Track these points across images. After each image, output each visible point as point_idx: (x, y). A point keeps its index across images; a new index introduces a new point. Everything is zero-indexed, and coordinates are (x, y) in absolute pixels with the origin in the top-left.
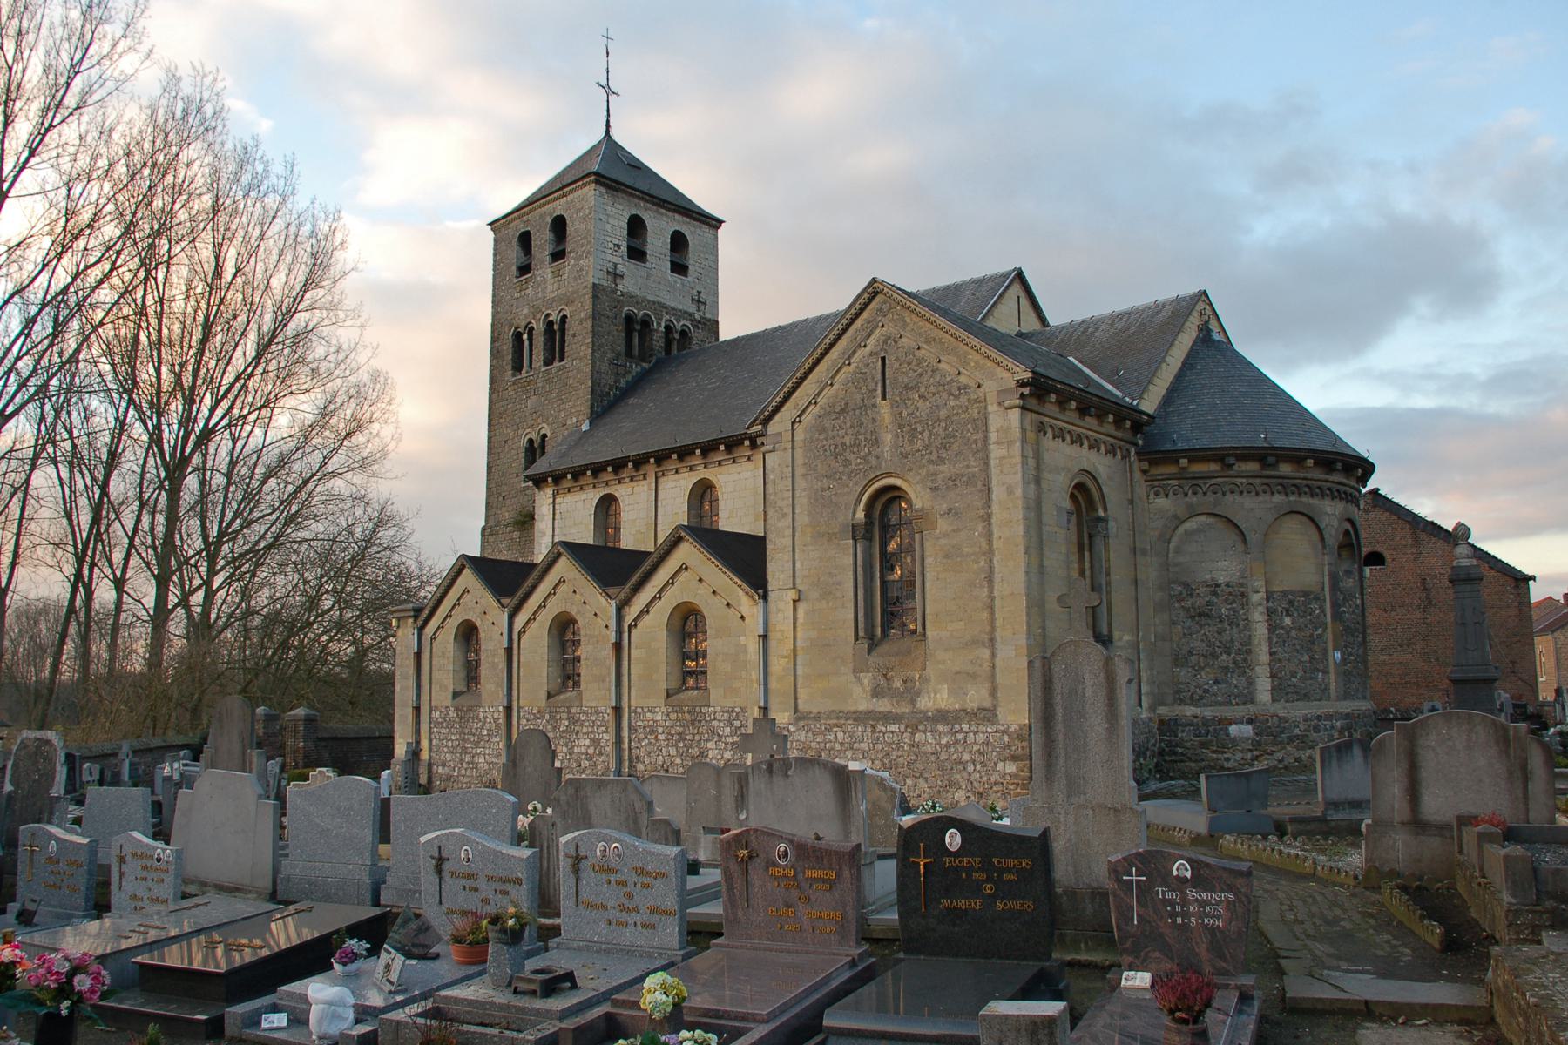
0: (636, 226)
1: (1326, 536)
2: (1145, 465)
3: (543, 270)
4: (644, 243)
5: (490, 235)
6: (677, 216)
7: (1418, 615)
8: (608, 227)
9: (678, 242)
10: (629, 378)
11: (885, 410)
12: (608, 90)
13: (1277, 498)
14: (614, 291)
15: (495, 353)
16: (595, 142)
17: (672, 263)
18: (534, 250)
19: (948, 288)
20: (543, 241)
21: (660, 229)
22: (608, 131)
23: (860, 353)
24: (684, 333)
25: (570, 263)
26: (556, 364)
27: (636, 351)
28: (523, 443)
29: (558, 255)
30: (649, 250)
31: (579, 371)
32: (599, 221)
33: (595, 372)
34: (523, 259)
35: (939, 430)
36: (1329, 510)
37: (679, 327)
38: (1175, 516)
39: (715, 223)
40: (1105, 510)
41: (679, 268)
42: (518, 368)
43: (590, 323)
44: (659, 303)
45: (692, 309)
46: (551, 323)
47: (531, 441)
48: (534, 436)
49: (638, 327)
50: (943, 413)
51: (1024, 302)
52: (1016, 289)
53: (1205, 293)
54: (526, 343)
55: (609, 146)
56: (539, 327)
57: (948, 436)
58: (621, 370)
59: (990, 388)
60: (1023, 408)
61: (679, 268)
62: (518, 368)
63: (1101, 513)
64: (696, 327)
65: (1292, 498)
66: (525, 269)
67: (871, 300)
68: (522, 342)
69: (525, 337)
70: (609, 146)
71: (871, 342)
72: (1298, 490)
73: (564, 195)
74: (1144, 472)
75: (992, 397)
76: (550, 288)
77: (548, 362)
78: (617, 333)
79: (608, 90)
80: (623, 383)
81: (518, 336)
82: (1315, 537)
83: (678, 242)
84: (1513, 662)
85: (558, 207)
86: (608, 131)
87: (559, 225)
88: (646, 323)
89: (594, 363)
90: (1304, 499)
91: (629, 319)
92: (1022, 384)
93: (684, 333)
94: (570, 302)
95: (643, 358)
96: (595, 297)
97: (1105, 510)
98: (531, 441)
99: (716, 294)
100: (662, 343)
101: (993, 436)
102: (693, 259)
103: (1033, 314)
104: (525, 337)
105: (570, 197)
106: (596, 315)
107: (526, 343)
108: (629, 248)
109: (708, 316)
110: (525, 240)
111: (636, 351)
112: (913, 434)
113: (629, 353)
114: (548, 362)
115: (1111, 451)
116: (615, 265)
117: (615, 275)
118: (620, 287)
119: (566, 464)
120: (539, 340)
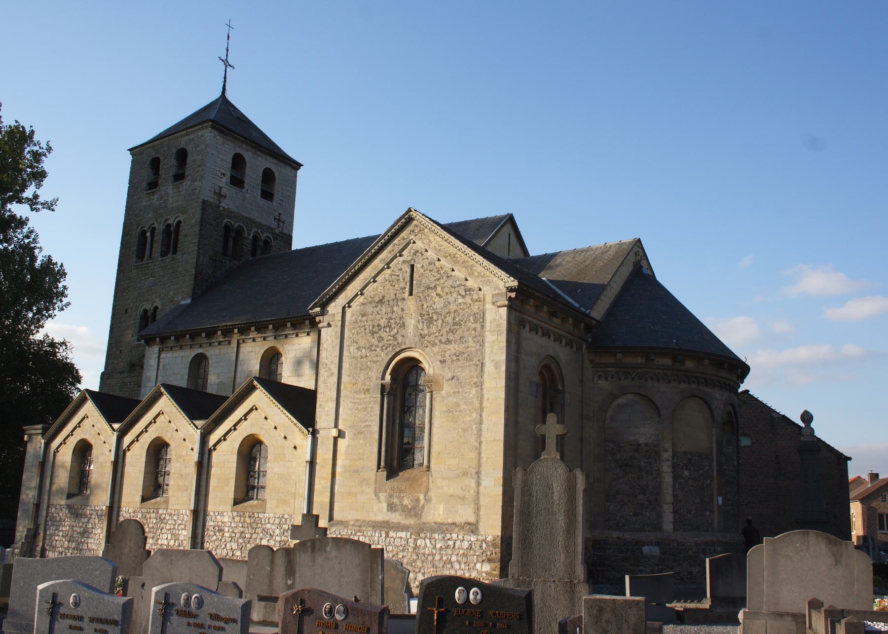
0: (238, 162)
3: (168, 188)
4: (243, 174)
5: (129, 158)
9: (268, 176)
12: (226, 63)
13: (683, 386)
14: (218, 207)
17: (262, 190)
20: (169, 166)
21: (256, 165)
24: (266, 242)
25: (186, 184)
26: (170, 255)
28: (140, 312)
29: (179, 177)
30: (247, 180)
33: (198, 265)
34: (152, 177)
35: (449, 319)
36: (718, 396)
37: (263, 237)
40: (563, 385)
41: (267, 195)
42: (140, 256)
43: (197, 228)
44: (250, 219)
45: (273, 224)
47: (146, 311)
49: (233, 235)
50: (453, 307)
51: (513, 238)
52: (508, 228)
54: (149, 239)
56: (160, 227)
61: (267, 195)
64: (275, 239)
65: (693, 386)
66: (153, 185)
68: (146, 237)
69: (148, 234)
75: (489, 299)
76: (170, 201)
77: (164, 254)
79: (226, 63)
81: (143, 233)
83: (268, 176)
85: (183, 142)
87: (182, 156)
88: (239, 232)
89: (198, 257)
91: (227, 228)
93: (266, 242)
96: (204, 210)
97: (563, 385)
98: (146, 311)
101: (488, 325)
102: (278, 189)
104: (148, 234)
105: (191, 137)
107: (149, 239)
108: (232, 177)
109: (285, 231)
110: (155, 164)
111: (230, 252)
112: (430, 321)
113: (225, 253)
114: (164, 254)
117: (220, 195)
118: (223, 204)
120: (159, 237)
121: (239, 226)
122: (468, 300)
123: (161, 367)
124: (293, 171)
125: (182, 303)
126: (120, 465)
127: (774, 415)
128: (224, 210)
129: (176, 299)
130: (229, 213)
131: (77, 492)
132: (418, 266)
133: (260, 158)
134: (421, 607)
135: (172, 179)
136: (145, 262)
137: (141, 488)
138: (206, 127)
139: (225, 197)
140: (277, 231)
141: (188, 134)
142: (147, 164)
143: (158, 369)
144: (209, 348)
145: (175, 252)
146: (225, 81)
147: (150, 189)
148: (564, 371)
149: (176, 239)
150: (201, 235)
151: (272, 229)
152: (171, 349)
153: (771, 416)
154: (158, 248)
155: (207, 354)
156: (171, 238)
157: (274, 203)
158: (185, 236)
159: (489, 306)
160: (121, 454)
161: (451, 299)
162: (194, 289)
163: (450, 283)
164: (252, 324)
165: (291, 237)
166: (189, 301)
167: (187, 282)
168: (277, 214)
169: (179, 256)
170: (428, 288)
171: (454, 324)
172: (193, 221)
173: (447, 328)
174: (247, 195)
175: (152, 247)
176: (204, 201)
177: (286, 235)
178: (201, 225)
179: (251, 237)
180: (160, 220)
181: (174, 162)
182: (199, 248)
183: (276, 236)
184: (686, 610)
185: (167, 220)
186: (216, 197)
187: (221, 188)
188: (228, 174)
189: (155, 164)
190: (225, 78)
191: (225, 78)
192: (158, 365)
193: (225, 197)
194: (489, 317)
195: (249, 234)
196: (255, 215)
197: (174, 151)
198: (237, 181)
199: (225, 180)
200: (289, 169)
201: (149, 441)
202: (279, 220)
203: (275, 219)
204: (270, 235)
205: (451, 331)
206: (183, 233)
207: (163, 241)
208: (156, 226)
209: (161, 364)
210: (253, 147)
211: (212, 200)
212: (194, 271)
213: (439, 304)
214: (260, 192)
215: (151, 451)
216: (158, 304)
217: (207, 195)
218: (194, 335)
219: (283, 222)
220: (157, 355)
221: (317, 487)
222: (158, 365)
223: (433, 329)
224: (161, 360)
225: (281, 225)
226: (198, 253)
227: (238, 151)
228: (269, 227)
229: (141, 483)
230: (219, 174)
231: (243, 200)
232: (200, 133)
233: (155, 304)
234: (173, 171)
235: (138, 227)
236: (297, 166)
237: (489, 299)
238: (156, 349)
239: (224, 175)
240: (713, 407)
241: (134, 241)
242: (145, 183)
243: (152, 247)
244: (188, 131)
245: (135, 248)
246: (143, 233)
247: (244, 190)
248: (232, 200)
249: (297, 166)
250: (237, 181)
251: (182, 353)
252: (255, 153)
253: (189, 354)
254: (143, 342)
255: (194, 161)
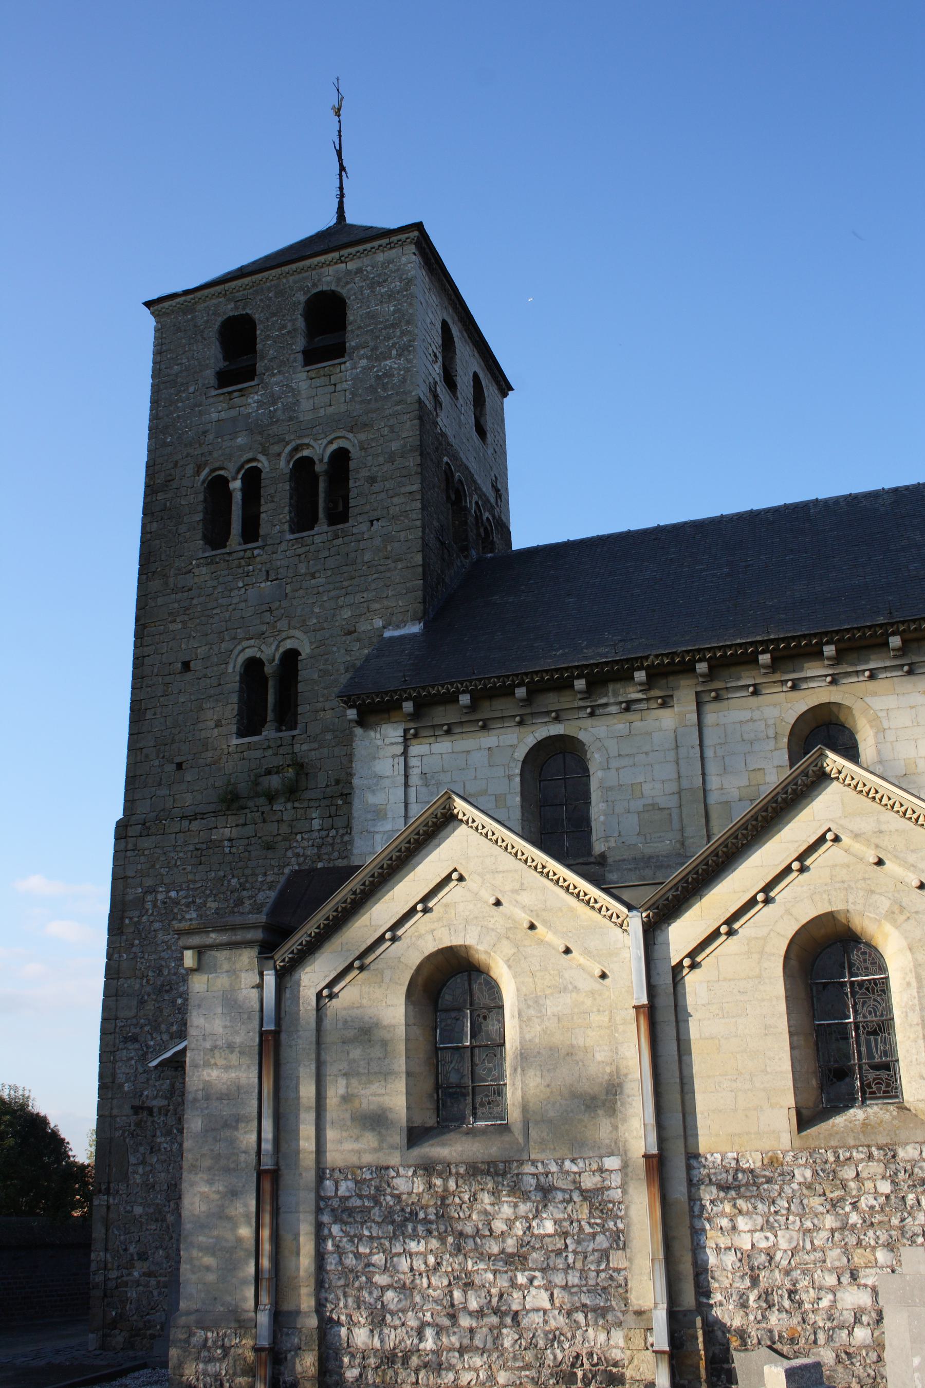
5: (148, 322)
26: (322, 526)
28: (235, 666)
47: (253, 666)
56: (276, 467)
68: (229, 494)
76: (306, 405)
81: (217, 487)
123: (414, 780)
125: (387, 634)
126: (666, 1015)
129: (363, 627)
131: (431, 1121)
134: (342, 1361)
137: (787, 1082)
138: (402, 243)
141: (340, 260)
142: (212, 333)
143: (406, 785)
144: (589, 722)
146: (342, 195)
147: (220, 386)
152: (448, 732)
155: (582, 736)
158: (372, 480)
160: (665, 980)
164: (829, 636)
169: (357, 525)
180: (276, 449)
184: (702, 1328)
192: (406, 776)
197: (302, 298)
201: (790, 929)
206: (364, 473)
208: (263, 463)
209: (415, 773)
212: (419, 558)
215: (793, 963)
218: (560, 683)
220: (400, 749)
221: (646, 1105)
222: (406, 776)
224: (413, 762)
229: (787, 1066)
232: (380, 257)
233: (288, 644)
235: (199, 469)
236: (511, 389)
238: (391, 734)
241: (191, 498)
244: (345, 252)
245: (199, 517)
249: (511, 389)
251: (489, 740)
253: (514, 742)
254: (352, 714)
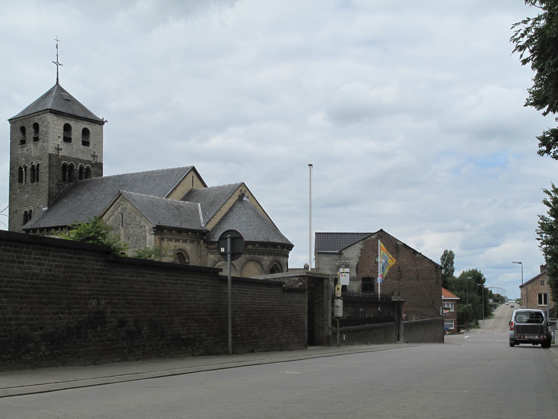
0: (67, 128)
1: (264, 267)
2: (206, 245)
3: (30, 145)
4: (70, 134)
5: (9, 125)
6: (85, 122)
7: (396, 281)
8: (55, 130)
9: (86, 132)
10: (64, 189)
11: (122, 231)
12: (57, 64)
13: (247, 256)
14: (58, 156)
15: (12, 175)
16: (52, 86)
17: (82, 141)
18: (27, 135)
19: (168, 170)
20: (30, 131)
21: (77, 128)
22: (57, 82)
23: (116, 212)
24: (88, 169)
25: (40, 143)
26: (35, 183)
27: (67, 178)
28: (23, 213)
29: (36, 139)
30: (73, 137)
31: (44, 187)
32: (54, 127)
33: (50, 189)
34: (22, 136)
35: (135, 238)
36: (266, 259)
37: (85, 167)
38: (215, 261)
39: (101, 123)
40: (189, 260)
41: (86, 143)
42: (20, 181)
43: (47, 169)
44: (77, 158)
45: (91, 159)
46: (33, 166)
47: (26, 212)
48: (27, 210)
49: (68, 169)
50: (136, 233)
51: (195, 178)
52: (192, 173)
53: (243, 183)
54: (24, 172)
55: (58, 88)
56: (29, 167)
57: (137, 240)
58: (61, 187)
59: (147, 228)
60: (155, 234)
61: (86, 143)
62: (20, 181)
63: (187, 261)
64: (93, 167)
65: (252, 256)
66: (23, 142)
67: (119, 196)
68: (22, 172)
69: (23, 170)
70: (58, 88)
71: (119, 209)
72: (255, 253)
73: (38, 115)
74: (207, 247)
75: (147, 231)
76: (33, 152)
77: (32, 181)
78: (58, 172)
79: (57, 64)
80: (61, 191)
81: (21, 169)
82: (260, 267)
83: (86, 132)
84: (433, 302)
85: (36, 120)
86: (57, 82)
87: (36, 127)
88: (71, 166)
89: (49, 185)
90: (256, 256)
91: (64, 166)
92: (154, 228)
93: (88, 169)
94: (40, 159)
95: (70, 181)
96: (50, 159)
97: (189, 260)
98: (26, 212)
99: (102, 152)
100: (78, 174)
101: (147, 241)
102: (92, 139)
103: (199, 181)
104: (23, 170)
105: (40, 116)
106: (50, 166)
107: (24, 172)
108: (64, 137)
109: (98, 161)
110: (23, 129)
111: (67, 178)
112: (129, 238)
113: (64, 179)
114: (32, 181)
115: (192, 242)
116: (58, 145)
117: (58, 149)
118: (60, 154)
119: (37, 226)
120: (29, 172)
121: (71, 164)
122: (141, 230)
124: (100, 126)
125: (43, 209)
127: (398, 243)
128: (61, 156)
130: (65, 158)
132: (124, 215)
133: (80, 123)
135: (32, 140)
136: (23, 185)
139: (61, 149)
140: (93, 162)
142: (19, 129)
145: (38, 181)
148: (189, 254)
149: (38, 174)
150: (49, 172)
151: (90, 162)
153: (397, 244)
154: (29, 178)
156: (35, 171)
157: (90, 147)
158: (42, 173)
159: (147, 234)
161: (135, 229)
162: (49, 202)
163: (135, 223)
165: (102, 164)
166: (46, 208)
167: (44, 198)
168: (92, 153)
169: (39, 183)
170: (128, 224)
171: (137, 240)
172: (45, 165)
173: (134, 242)
174: (74, 146)
175: (26, 178)
176: (50, 154)
177: (99, 163)
178: (49, 167)
179: (78, 169)
181: (32, 130)
182: (49, 180)
183: (93, 165)
185: (32, 163)
186: (56, 151)
187: (58, 145)
188: (62, 136)
189: (23, 129)
190: (58, 73)
191: (58, 73)
193: (61, 149)
194: (148, 238)
195: (77, 167)
196: (80, 156)
197: (32, 124)
198: (67, 139)
199: (61, 139)
200: (97, 125)
202: (94, 156)
203: (92, 156)
204: (89, 165)
205: (136, 243)
207: (31, 174)
208: (27, 165)
210: (75, 118)
211: (54, 153)
212: (48, 193)
213: (131, 232)
214: (81, 142)
216: (32, 208)
217: (52, 151)
219: (97, 157)
223: (130, 242)
225: (96, 158)
226: (49, 182)
227: (67, 122)
228: (88, 161)
230: (57, 137)
231: (72, 149)
234: (32, 136)
235: (17, 165)
237: (147, 231)
239: (60, 137)
240: (262, 264)
241: (16, 172)
242: (19, 141)
243: (26, 178)
246: (21, 169)
247: (72, 143)
248: (66, 151)
250: (67, 139)
252: (76, 121)
255: (43, 131)
